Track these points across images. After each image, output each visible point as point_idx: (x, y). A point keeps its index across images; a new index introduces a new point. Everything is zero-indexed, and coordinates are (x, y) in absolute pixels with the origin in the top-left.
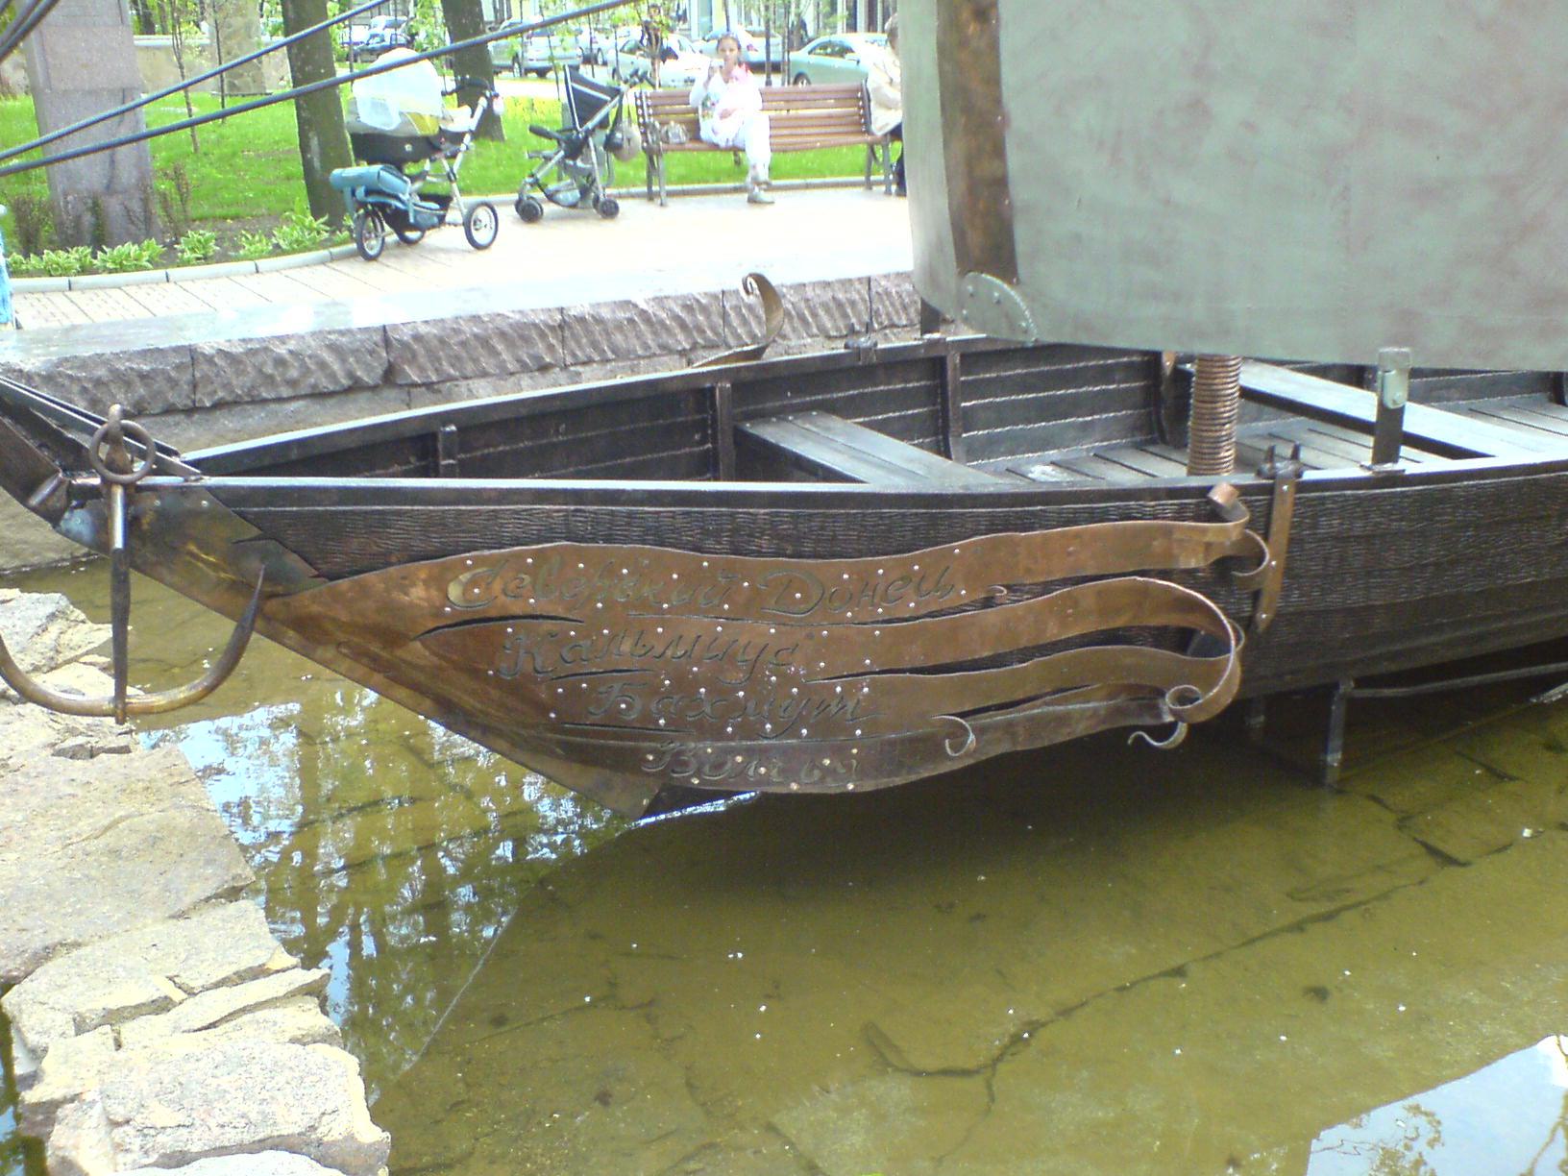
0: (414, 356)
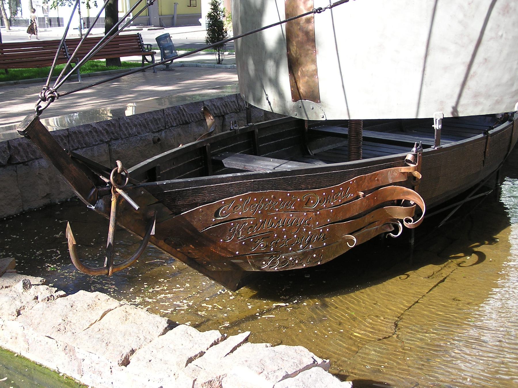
0: (19, 152)
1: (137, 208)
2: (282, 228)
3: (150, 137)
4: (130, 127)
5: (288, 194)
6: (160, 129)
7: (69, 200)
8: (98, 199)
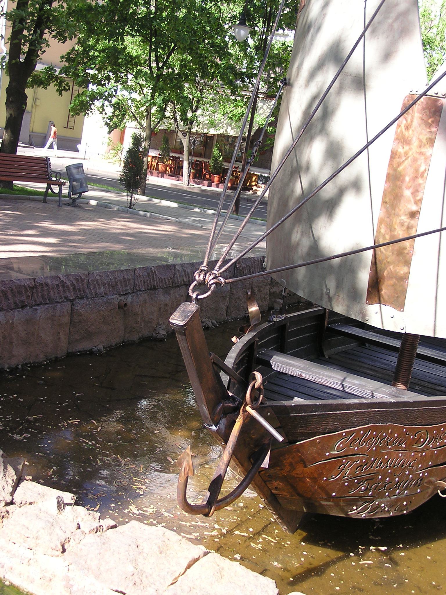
1: (280, 438)
2: (389, 469)
3: (116, 299)
4: (99, 285)
5: (404, 430)
6: (128, 292)
7: (20, 367)
8: (221, 419)
